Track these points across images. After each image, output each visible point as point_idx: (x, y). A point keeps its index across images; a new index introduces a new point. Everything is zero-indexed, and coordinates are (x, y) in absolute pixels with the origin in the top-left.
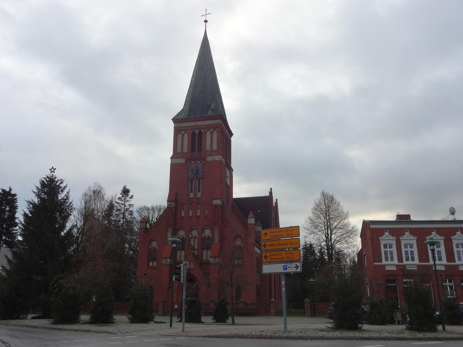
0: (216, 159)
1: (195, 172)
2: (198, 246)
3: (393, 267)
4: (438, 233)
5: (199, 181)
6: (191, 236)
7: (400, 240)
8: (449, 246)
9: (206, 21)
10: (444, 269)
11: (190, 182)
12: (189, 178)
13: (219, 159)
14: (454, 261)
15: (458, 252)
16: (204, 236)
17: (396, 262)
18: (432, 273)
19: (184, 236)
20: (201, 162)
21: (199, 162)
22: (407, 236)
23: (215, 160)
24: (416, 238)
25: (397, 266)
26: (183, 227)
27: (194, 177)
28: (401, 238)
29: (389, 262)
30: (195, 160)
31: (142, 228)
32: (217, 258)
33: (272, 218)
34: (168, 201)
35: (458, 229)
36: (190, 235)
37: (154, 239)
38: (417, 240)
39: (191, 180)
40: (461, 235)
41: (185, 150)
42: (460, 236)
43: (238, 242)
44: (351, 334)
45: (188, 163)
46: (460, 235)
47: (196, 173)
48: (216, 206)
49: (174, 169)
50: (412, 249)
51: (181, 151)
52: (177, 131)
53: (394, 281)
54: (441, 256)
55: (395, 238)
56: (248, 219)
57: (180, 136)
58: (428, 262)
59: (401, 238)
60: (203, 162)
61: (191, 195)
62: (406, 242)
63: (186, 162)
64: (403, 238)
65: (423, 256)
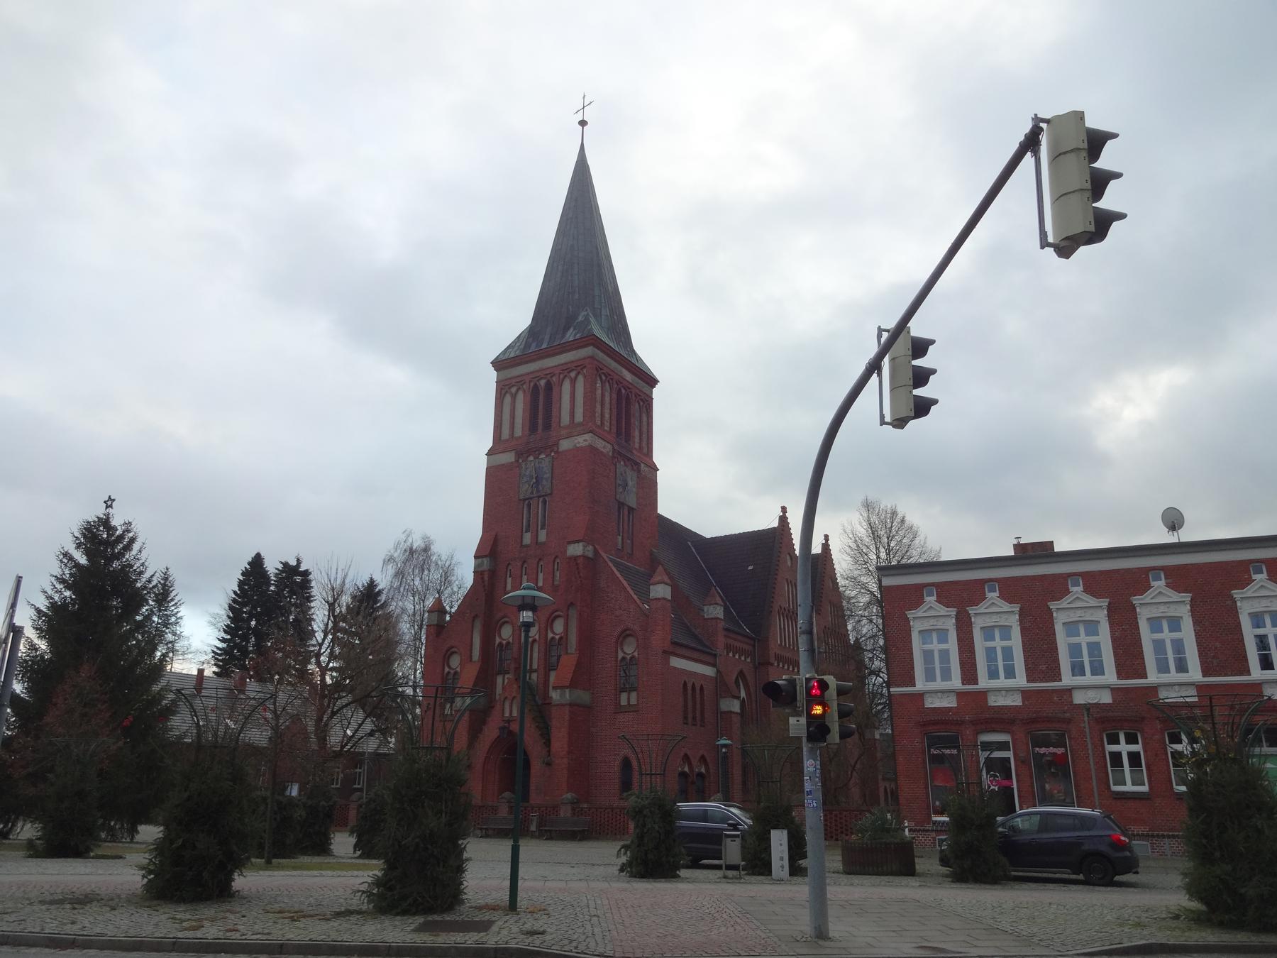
0: (579, 443)
1: (534, 480)
3: (1012, 695)
4: (1089, 590)
5: (545, 502)
7: (1135, 608)
8: (1123, 627)
9: (583, 123)
10: (1111, 702)
11: (525, 506)
12: (522, 497)
13: (587, 443)
14: (1057, 676)
15: (1262, 642)
16: (552, 635)
17: (956, 683)
18: (1068, 715)
19: (511, 640)
20: (547, 456)
21: (544, 456)
22: (1156, 593)
23: (578, 445)
24: (1105, 602)
25: (960, 695)
26: (509, 618)
27: (532, 493)
28: (972, 610)
29: (1002, 682)
30: (535, 451)
31: (430, 626)
32: (567, 691)
34: (476, 557)
35: (992, 583)
37: (454, 650)
38: (1022, 614)
39: (527, 502)
40: (1271, 585)
41: (518, 433)
42: (1160, 593)
43: (630, 649)
44: (317, 860)
45: (521, 461)
46: (1080, 596)
47: (538, 482)
48: (575, 558)
49: (496, 479)
50: (1176, 635)
51: (509, 435)
52: (503, 390)
53: (952, 742)
54: (1014, 664)
55: (953, 612)
56: (651, 587)
57: (508, 399)
58: (1055, 681)
59: (972, 610)
60: (553, 454)
61: (527, 539)
62: (1156, 612)
63: (517, 461)
64: (1142, 599)
65: (1129, 658)
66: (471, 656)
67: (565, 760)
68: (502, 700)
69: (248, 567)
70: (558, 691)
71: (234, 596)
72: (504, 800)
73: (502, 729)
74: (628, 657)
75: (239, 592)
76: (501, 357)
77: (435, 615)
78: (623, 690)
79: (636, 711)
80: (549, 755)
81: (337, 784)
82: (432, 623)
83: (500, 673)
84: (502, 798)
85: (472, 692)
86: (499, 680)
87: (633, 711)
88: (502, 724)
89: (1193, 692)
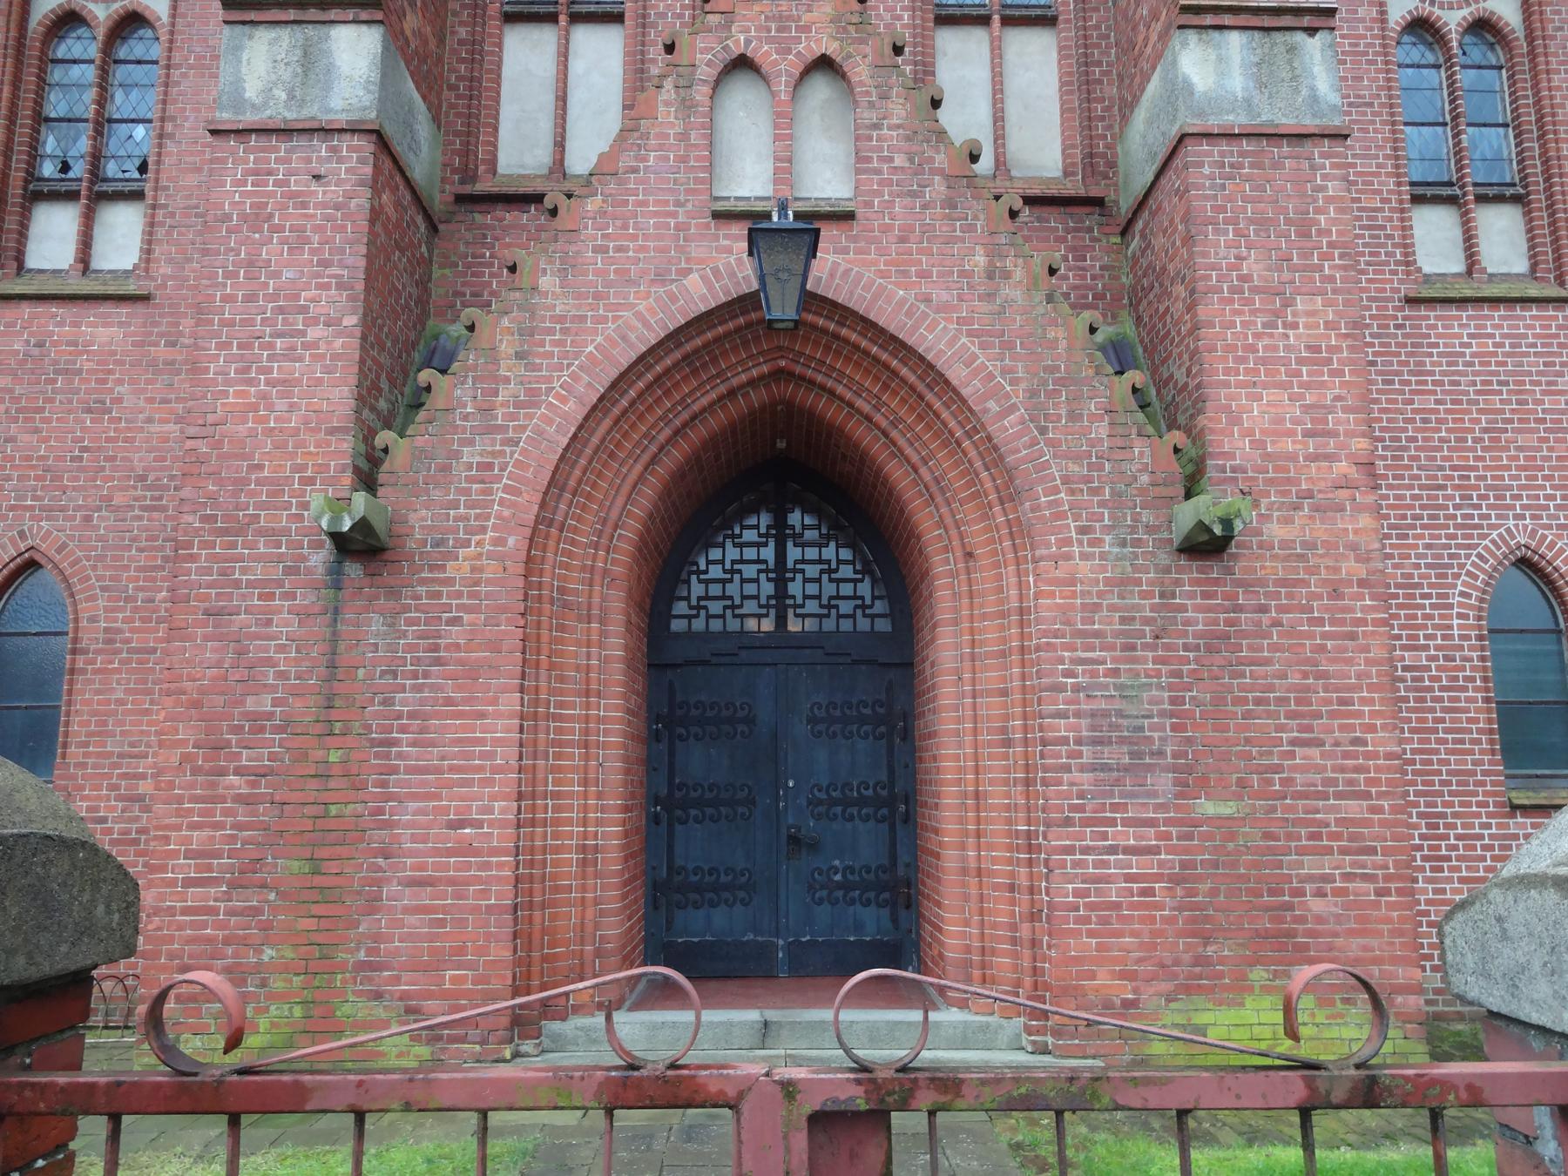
70: (1235, 38)
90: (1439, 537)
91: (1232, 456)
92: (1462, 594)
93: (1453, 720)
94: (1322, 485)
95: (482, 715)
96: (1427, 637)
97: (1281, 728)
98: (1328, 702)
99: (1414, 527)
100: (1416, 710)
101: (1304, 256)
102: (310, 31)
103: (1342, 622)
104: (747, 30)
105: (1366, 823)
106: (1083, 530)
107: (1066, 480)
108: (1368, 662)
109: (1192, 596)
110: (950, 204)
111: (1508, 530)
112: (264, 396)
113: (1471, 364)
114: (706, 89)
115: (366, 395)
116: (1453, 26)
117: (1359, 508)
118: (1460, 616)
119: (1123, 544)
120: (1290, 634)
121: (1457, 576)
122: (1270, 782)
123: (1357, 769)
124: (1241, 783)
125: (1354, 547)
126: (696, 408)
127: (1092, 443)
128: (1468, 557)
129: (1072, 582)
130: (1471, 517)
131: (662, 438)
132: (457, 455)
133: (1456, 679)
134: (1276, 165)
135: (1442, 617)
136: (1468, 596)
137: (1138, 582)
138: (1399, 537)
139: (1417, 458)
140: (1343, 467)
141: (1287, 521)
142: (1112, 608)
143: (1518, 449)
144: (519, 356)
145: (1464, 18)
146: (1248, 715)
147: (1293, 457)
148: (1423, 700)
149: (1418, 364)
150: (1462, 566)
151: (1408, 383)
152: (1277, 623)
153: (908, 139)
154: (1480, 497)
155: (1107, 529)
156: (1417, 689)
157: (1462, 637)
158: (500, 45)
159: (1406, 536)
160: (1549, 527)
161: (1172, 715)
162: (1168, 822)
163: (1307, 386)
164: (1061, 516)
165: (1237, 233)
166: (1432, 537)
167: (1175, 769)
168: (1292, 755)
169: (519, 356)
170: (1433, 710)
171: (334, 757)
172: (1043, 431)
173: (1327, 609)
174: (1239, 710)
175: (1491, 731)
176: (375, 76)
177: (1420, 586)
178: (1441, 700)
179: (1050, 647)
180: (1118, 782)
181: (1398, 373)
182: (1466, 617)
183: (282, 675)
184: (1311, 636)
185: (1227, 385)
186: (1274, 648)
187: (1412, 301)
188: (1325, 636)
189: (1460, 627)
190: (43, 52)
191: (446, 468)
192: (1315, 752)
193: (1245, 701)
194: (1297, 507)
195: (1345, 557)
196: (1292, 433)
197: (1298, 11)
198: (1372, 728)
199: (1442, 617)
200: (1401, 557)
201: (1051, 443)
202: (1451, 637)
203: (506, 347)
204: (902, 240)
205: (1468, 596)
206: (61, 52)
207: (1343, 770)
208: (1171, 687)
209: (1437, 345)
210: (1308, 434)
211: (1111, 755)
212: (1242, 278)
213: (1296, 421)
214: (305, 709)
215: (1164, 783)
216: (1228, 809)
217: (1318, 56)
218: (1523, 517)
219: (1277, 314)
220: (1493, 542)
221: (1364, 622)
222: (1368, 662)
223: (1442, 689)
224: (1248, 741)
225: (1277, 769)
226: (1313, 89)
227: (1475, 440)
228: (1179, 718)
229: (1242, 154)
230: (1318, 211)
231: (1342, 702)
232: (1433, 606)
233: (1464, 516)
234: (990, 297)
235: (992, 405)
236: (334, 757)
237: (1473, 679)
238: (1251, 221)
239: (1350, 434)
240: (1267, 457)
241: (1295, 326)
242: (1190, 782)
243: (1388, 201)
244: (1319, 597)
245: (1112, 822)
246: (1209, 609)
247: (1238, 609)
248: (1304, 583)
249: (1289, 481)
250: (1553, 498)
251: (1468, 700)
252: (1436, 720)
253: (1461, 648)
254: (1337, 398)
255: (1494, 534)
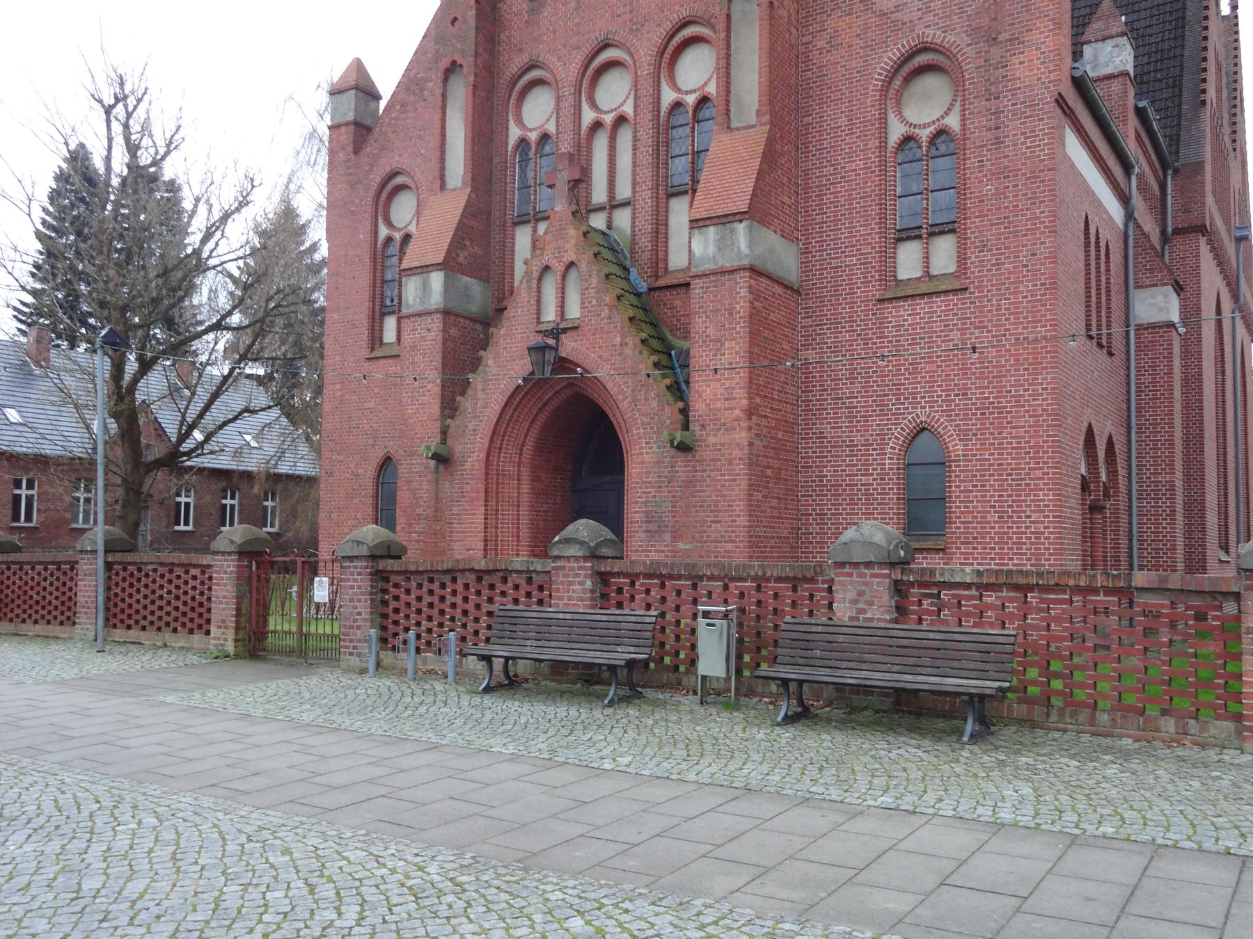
2: (634, 184)
6: (588, 116)
19: (551, 128)
32: (741, 228)
33: (1211, 55)
36: (585, 107)
37: (399, 180)
66: (442, 177)
67: (742, 436)
68: (536, 275)
69: (64, 166)
70: (712, 229)
71: (43, 215)
72: (574, 551)
73: (538, 350)
74: (924, 134)
75: (51, 209)
76: (478, 101)
77: (350, 98)
78: (906, 235)
79: (954, 292)
80: (686, 427)
81: (186, 523)
82: (343, 120)
83: (521, 221)
84: (567, 541)
85: (449, 265)
86: (522, 239)
87: (946, 292)
88: (538, 340)
89: (321, 583)
90: (883, 420)
91: (698, 411)
92: (892, 448)
93: (882, 509)
94: (729, 420)
95: (474, 514)
96: (873, 469)
97: (708, 516)
98: (724, 506)
99: (872, 416)
100: (864, 504)
101: (729, 324)
102: (425, 275)
103: (732, 475)
104: (548, 255)
105: (734, 552)
106: (647, 443)
107: (642, 424)
108: (740, 490)
109: (681, 467)
110: (610, 318)
111: (917, 415)
112: (417, 409)
113: (907, 330)
114: (535, 281)
115: (443, 408)
116: (924, 139)
117: (741, 428)
118: (889, 458)
119: (659, 448)
120: (713, 480)
121: (890, 439)
122: (702, 537)
123: (733, 532)
124: (693, 537)
125: (738, 445)
126: (545, 400)
127: (652, 409)
128: (896, 429)
129: (643, 463)
130: (900, 409)
131: (535, 412)
132: (466, 427)
133: (885, 489)
134: (723, 285)
135: (881, 459)
136: (894, 448)
137: (664, 462)
138: (865, 421)
139: (876, 381)
140: (737, 412)
141: (715, 435)
142: (655, 473)
143: (926, 372)
144: (483, 390)
145: (931, 132)
146: (697, 512)
147: (719, 410)
148: (869, 499)
149: (881, 333)
150: (892, 434)
151: (876, 343)
152: (709, 476)
153: (597, 292)
154: (905, 399)
155: (655, 443)
156: (866, 494)
157: (890, 469)
158: (513, 238)
159: (868, 421)
160: (938, 411)
161: (672, 512)
162: (669, 551)
163: (726, 379)
164: (640, 438)
165: (707, 317)
166: (880, 420)
167: (672, 532)
168: (711, 526)
169: (483, 390)
170: (873, 504)
171: (438, 528)
172: (636, 405)
173: (727, 470)
174: (694, 510)
175: (950, 512)
176: (442, 290)
177: (872, 445)
178: (877, 499)
179: (635, 487)
180: (652, 537)
181: (871, 339)
182: (892, 459)
183: (425, 502)
184: (720, 481)
185: (698, 381)
186: (708, 486)
187: (881, 301)
188: (725, 480)
189: (889, 464)
190: (383, 251)
191: (464, 431)
192: (718, 525)
193: (696, 506)
194: (719, 430)
195: (734, 449)
196: (720, 399)
197: (733, 214)
198: (739, 516)
199: (881, 459)
200: (865, 431)
201: (639, 410)
202: (884, 469)
203: (479, 388)
204: (594, 334)
205: (894, 448)
206: (389, 253)
207: (727, 532)
208: (672, 502)
209: (891, 322)
210: (726, 399)
211: (653, 527)
212: (707, 336)
213: (722, 395)
214: (430, 512)
215: (667, 537)
216: (687, 547)
217: (742, 232)
218: (925, 407)
219: (718, 350)
220: (909, 421)
221: (739, 475)
222: (740, 490)
223: (878, 494)
224: (696, 521)
225: (705, 532)
226: (739, 248)
227: (905, 370)
228: (674, 512)
229: (710, 282)
230: (737, 303)
231: (729, 506)
232: (877, 454)
233: (896, 409)
234: (621, 354)
235: (621, 397)
236: (438, 528)
237: (893, 489)
238: (712, 311)
239: (741, 398)
240: (711, 410)
241: (724, 354)
242: (676, 537)
243: (875, 248)
244: (724, 465)
245: (651, 551)
246: (687, 472)
247: (696, 471)
248: (720, 460)
249: (717, 419)
250: (941, 396)
251: (889, 499)
252: (874, 509)
253: (889, 474)
254: (737, 384)
255: (910, 417)
